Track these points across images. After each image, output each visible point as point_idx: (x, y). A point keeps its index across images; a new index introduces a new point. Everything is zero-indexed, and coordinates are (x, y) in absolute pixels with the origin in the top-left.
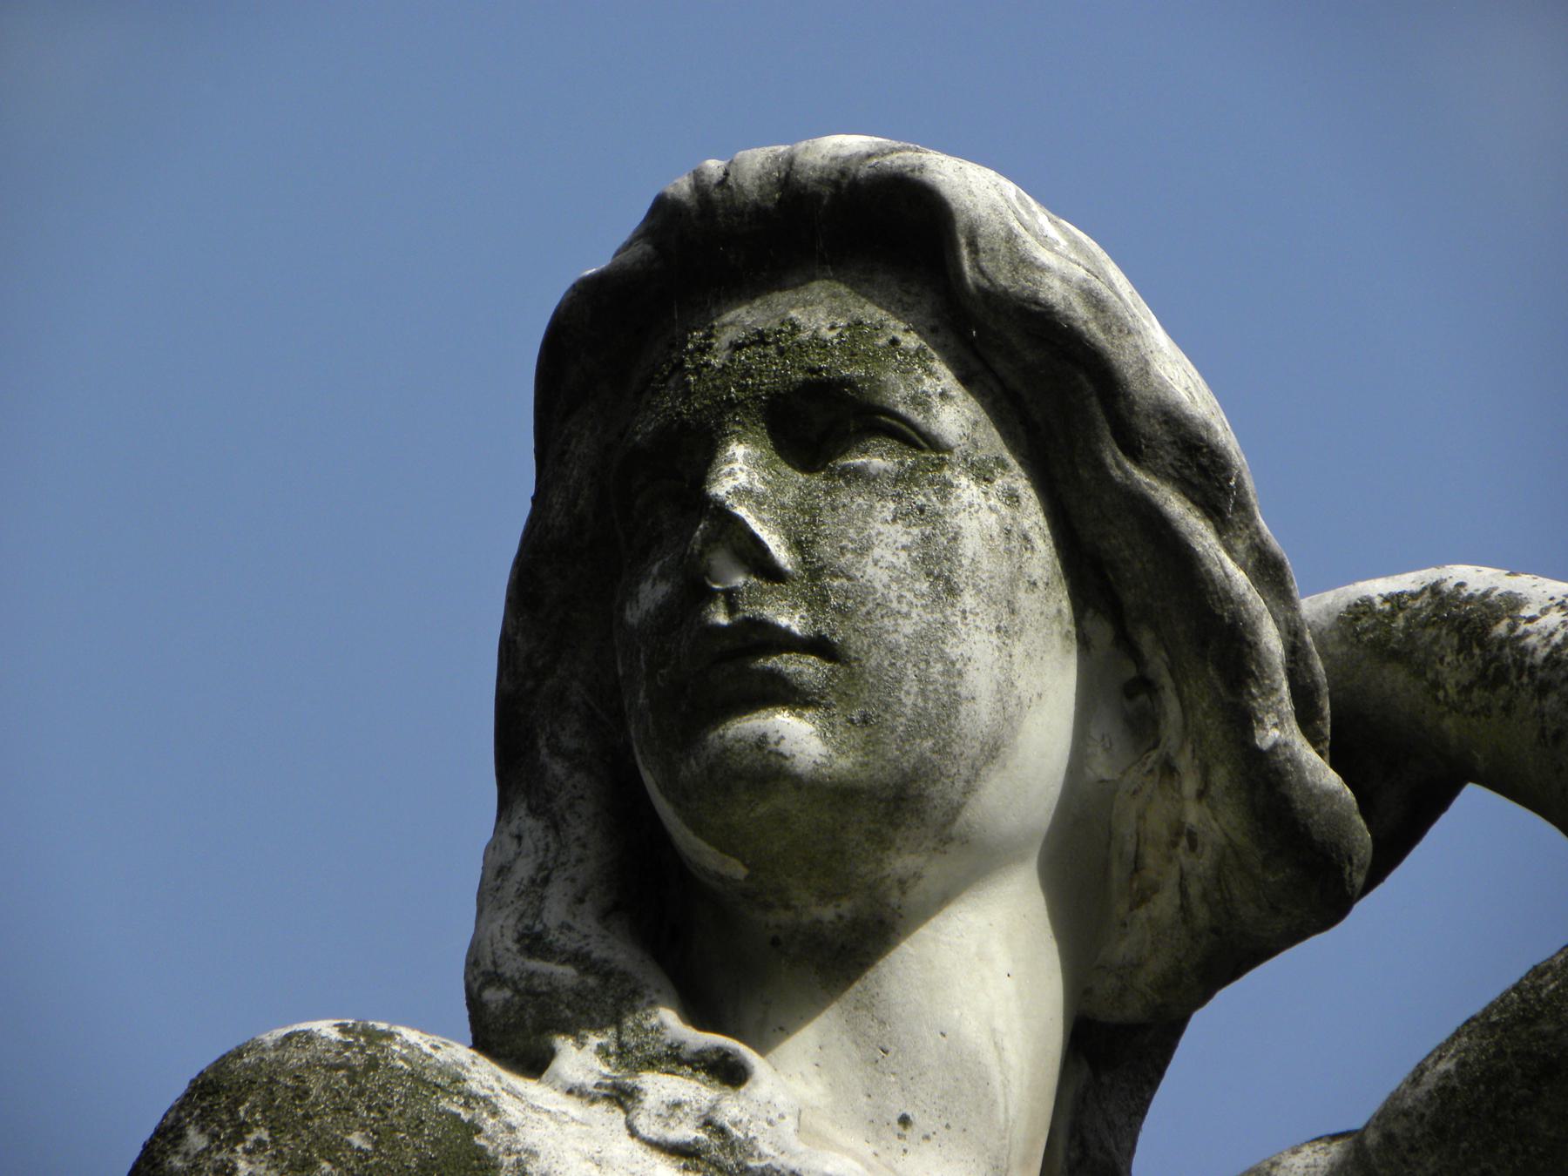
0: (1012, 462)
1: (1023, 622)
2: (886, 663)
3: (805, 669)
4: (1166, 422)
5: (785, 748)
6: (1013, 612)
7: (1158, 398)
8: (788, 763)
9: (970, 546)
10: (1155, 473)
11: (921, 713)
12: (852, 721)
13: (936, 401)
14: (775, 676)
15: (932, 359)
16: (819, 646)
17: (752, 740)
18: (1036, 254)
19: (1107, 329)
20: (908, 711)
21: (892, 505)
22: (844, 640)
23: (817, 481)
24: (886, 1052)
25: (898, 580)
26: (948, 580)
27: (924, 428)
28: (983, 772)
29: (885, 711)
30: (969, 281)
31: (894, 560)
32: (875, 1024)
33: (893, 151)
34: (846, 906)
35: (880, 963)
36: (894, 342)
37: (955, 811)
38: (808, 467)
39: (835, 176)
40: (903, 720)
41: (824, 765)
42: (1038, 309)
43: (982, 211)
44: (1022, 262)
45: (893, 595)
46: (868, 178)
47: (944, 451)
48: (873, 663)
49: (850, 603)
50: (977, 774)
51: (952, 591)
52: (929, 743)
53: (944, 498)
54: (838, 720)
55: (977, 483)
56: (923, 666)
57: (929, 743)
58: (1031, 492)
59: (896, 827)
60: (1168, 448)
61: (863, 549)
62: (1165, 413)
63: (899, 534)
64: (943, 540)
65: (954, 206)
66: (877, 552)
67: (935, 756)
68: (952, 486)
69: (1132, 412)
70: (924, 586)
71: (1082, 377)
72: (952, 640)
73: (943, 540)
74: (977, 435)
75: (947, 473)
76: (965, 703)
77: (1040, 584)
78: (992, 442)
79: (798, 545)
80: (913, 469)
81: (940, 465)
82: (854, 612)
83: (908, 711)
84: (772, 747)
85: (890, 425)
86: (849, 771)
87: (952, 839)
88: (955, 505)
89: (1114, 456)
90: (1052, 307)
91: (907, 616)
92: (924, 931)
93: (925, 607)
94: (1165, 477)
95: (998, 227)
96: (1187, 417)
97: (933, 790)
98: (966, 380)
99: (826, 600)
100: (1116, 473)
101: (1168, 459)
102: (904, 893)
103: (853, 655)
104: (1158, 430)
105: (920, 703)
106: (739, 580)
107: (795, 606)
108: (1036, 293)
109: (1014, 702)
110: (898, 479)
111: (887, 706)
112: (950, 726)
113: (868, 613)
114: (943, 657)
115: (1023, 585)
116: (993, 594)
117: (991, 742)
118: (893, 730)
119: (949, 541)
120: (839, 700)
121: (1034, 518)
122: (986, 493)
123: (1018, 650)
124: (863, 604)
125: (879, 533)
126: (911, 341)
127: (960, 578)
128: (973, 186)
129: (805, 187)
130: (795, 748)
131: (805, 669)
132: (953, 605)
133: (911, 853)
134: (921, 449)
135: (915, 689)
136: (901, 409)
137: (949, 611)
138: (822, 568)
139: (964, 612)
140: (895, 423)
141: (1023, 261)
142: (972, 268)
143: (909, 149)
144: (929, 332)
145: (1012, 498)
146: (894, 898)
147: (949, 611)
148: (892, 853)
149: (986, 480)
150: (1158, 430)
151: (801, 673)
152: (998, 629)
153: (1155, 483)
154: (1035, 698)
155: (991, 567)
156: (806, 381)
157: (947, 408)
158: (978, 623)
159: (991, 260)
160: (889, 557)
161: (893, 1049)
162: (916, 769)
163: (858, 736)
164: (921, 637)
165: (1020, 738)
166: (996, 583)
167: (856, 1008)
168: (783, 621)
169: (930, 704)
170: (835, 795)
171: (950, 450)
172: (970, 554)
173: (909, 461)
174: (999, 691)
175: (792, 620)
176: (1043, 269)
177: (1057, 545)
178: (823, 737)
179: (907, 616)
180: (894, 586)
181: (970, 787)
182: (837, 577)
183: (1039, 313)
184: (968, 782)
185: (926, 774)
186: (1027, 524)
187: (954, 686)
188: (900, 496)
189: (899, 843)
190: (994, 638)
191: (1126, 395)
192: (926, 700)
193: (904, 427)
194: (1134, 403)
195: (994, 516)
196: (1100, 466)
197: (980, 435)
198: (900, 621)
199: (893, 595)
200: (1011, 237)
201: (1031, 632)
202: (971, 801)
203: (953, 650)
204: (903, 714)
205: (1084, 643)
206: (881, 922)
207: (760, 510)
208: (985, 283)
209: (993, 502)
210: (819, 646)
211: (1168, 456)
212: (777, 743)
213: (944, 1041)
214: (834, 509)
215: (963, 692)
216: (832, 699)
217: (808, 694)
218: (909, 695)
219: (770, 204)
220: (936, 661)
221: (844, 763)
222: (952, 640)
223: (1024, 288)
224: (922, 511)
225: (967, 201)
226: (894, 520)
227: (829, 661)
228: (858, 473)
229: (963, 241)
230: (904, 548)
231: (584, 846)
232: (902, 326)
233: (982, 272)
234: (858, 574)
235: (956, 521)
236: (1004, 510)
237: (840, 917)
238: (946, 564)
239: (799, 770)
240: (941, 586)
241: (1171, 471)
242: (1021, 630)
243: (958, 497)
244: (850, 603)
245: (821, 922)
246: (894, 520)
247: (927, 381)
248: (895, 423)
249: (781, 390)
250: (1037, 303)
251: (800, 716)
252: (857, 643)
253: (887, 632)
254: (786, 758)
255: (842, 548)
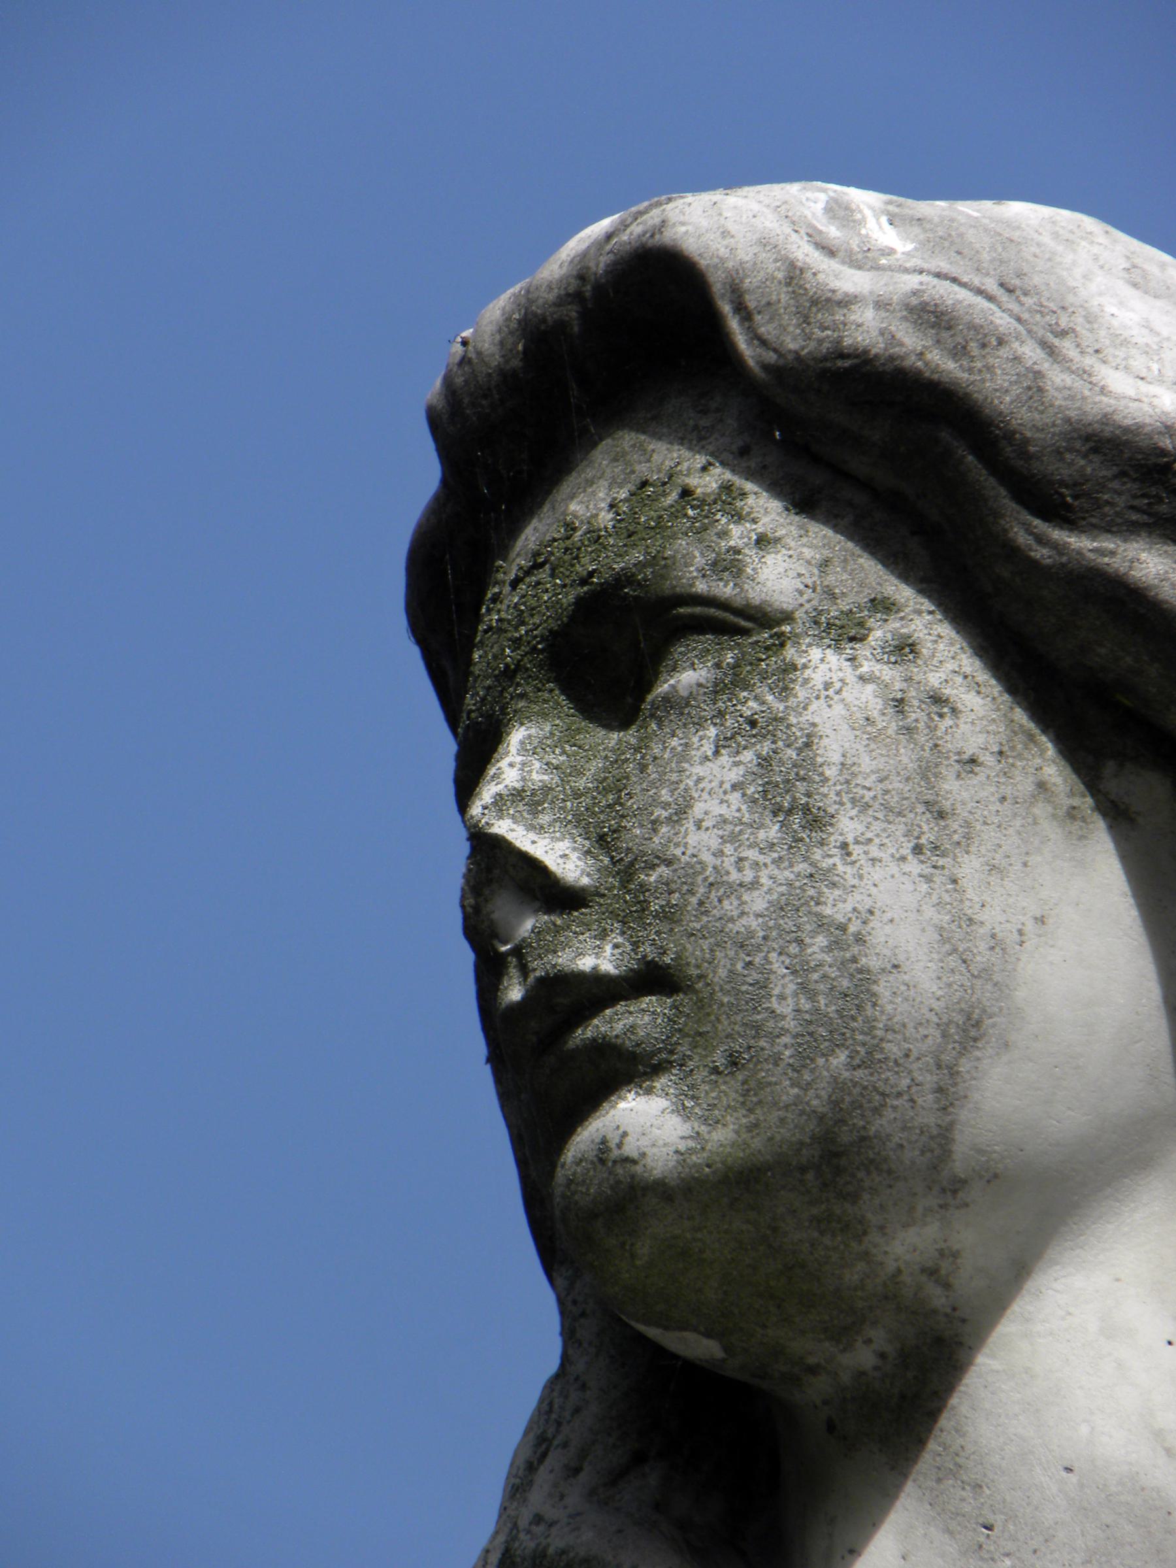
0: (903, 593)
1: (967, 824)
2: (739, 966)
3: (636, 1021)
4: (1095, 450)
5: (630, 1148)
6: (941, 815)
7: (1068, 420)
8: (638, 1169)
9: (833, 749)
10: (1109, 528)
11: (811, 1021)
12: (716, 1071)
13: (751, 555)
14: (603, 1048)
15: (743, 495)
16: (652, 979)
17: (591, 1155)
18: (834, 284)
19: (959, 352)
20: (790, 1024)
21: (712, 732)
22: (679, 957)
23: (630, 736)
24: (989, 1528)
25: (733, 838)
26: (806, 809)
27: (738, 602)
28: (964, 1066)
29: (756, 1037)
30: (751, 363)
31: (723, 810)
32: (967, 1494)
33: (624, 225)
34: (879, 1337)
35: (954, 1401)
36: (686, 493)
37: (941, 1141)
38: (624, 725)
39: (574, 285)
40: (786, 1039)
41: (691, 1151)
42: (847, 363)
43: (745, 254)
44: (817, 304)
45: (728, 863)
46: (607, 272)
47: (779, 623)
48: (722, 973)
49: (675, 898)
50: (953, 1072)
51: (817, 821)
52: (842, 1057)
53: (784, 691)
54: (701, 1075)
55: (838, 649)
56: (793, 949)
57: (842, 1057)
58: (946, 630)
59: (854, 1198)
60: (1115, 485)
61: (681, 812)
62: (1088, 438)
63: (726, 770)
64: (792, 753)
65: (703, 263)
66: (698, 809)
67: (860, 1073)
68: (795, 668)
69: (1028, 457)
70: (773, 831)
71: (945, 435)
72: (831, 895)
73: (792, 753)
74: (831, 579)
75: (790, 652)
76: (883, 979)
77: (988, 759)
78: (869, 574)
79: (603, 841)
80: (736, 666)
81: (781, 641)
82: (681, 908)
83: (790, 1024)
84: (615, 1153)
85: (692, 616)
86: (733, 1144)
87: (964, 1182)
88: (801, 693)
89: (1029, 530)
90: (866, 352)
91: (755, 884)
92: (1007, 1329)
93: (778, 861)
94: (1129, 529)
95: (771, 267)
96: (1126, 430)
97: (882, 1124)
98: (804, 502)
99: (644, 906)
100: (1041, 554)
101: (1121, 501)
102: (947, 1286)
103: (694, 972)
104: (1092, 468)
105: (805, 1005)
106: (527, 925)
107: (603, 935)
108: (839, 341)
109: (982, 946)
110: (718, 689)
111: (757, 1028)
112: (867, 1021)
113: (701, 903)
114: (822, 924)
115: (949, 772)
116: (894, 801)
117: (960, 1019)
118: (777, 1059)
119: (800, 751)
120: (694, 1046)
121: (950, 666)
122: (852, 659)
123: (969, 867)
124: (691, 892)
125: (700, 780)
126: (708, 482)
127: (828, 797)
128: (729, 225)
129: (544, 320)
130: (644, 1142)
131: (636, 1021)
132: (822, 843)
133: (905, 1226)
134: (745, 632)
135: (792, 987)
136: (701, 587)
137: (817, 854)
138: (632, 864)
139: (844, 846)
140: (698, 610)
141: (815, 302)
142: (749, 343)
143: (641, 213)
144: (738, 456)
145: (904, 649)
146: (938, 1298)
147: (817, 854)
148: (874, 1236)
149: (852, 639)
150: (1092, 468)
151: (632, 1028)
152: (918, 850)
153: (1108, 544)
154: (1030, 927)
155: (880, 763)
156: (579, 601)
157: (770, 559)
158: (874, 852)
159: (771, 320)
160: (718, 810)
161: (998, 1520)
162: (835, 1104)
163: (730, 1089)
164: (780, 908)
165: (1020, 994)
166: (896, 784)
167: (939, 1480)
168: (586, 963)
169: (822, 1001)
170: (731, 1186)
171: (788, 617)
172: (836, 758)
173: (729, 658)
174: (944, 940)
175: (597, 956)
176: (847, 302)
177: (1012, 688)
178: (682, 1111)
179: (755, 884)
180: (729, 849)
181: (948, 1095)
182: (653, 867)
183: (847, 371)
184: (940, 1090)
185: (856, 1105)
186: (934, 679)
187: (854, 960)
188: (721, 714)
189: (873, 1218)
190: (914, 866)
191: (1009, 435)
192: (812, 996)
193: (712, 611)
194: (1026, 441)
195: (870, 688)
196: (1013, 552)
197: (836, 577)
198: (745, 897)
199: (728, 863)
200: (794, 274)
201: (990, 835)
202: (963, 1115)
203: (836, 907)
204: (784, 1031)
205: (1118, 815)
206: (939, 1341)
207: (535, 813)
208: (771, 357)
209: (865, 668)
210: (652, 979)
211: (1119, 496)
212: (620, 1146)
213: (1073, 1478)
214: (643, 768)
215: (872, 962)
216: (684, 1049)
217: (653, 1054)
218: (786, 1002)
219: (516, 363)
220: (814, 934)
221: (721, 1136)
222: (831, 895)
223: (820, 341)
224: (753, 723)
225: (720, 247)
226: (717, 753)
227: (669, 995)
228: (670, 702)
229: (726, 308)
230: (735, 787)
231: (584, 1387)
232: (700, 460)
233: (764, 343)
234: (678, 852)
235: (807, 716)
236: (887, 673)
237: (882, 1356)
238: (801, 787)
239: (657, 1173)
240: (796, 820)
241: (1134, 517)
242: (967, 837)
243: (806, 681)
244: (675, 898)
245: (863, 1374)
246: (717, 753)
247: (736, 530)
248: (698, 610)
249: (553, 625)
250: (842, 356)
251: (649, 1091)
252: (696, 951)
253: (732, 920)
254: (634, 1162)
255: (654, 822)
